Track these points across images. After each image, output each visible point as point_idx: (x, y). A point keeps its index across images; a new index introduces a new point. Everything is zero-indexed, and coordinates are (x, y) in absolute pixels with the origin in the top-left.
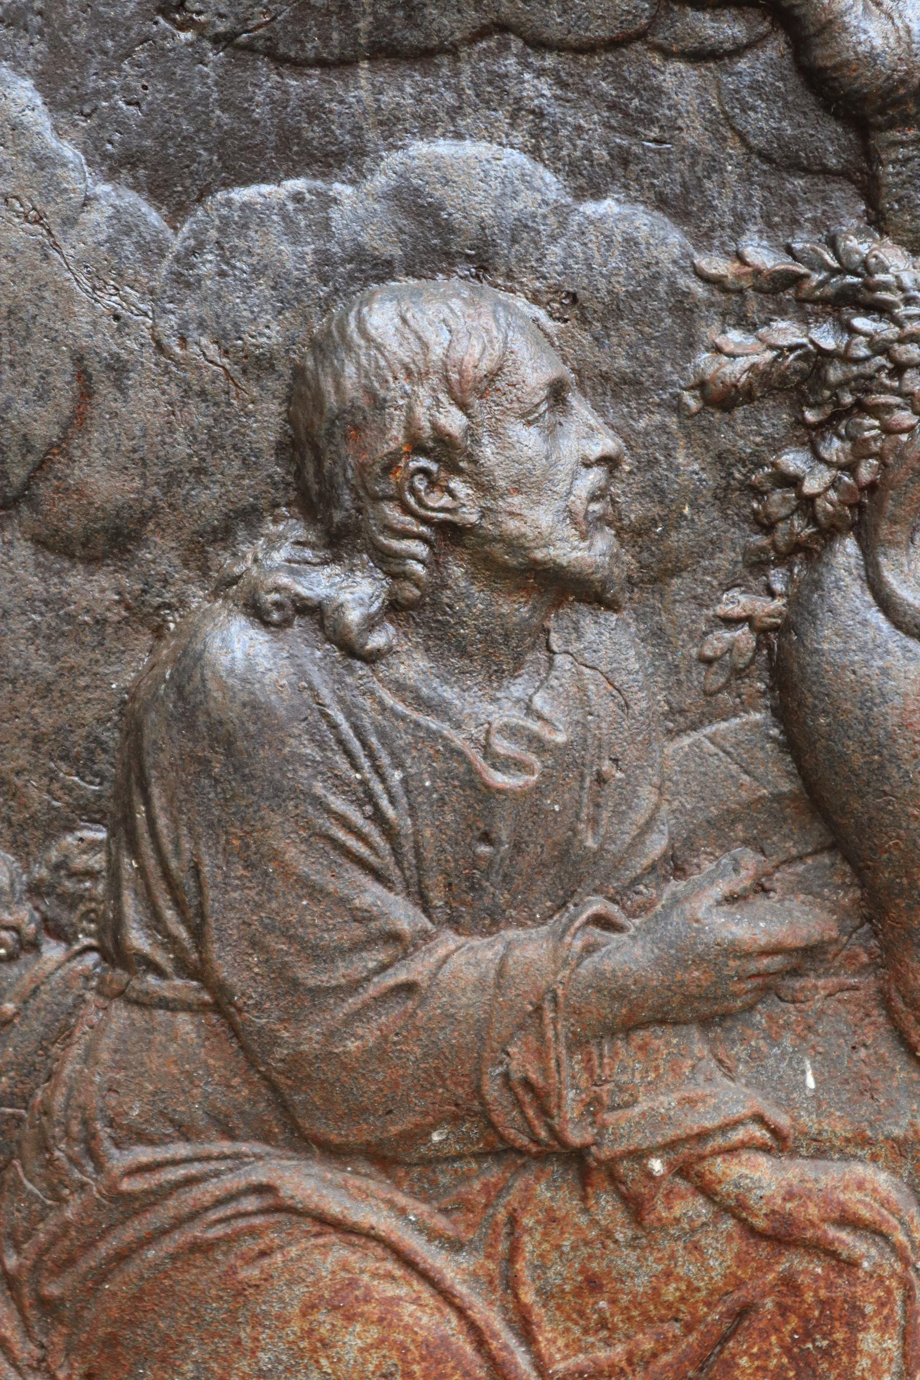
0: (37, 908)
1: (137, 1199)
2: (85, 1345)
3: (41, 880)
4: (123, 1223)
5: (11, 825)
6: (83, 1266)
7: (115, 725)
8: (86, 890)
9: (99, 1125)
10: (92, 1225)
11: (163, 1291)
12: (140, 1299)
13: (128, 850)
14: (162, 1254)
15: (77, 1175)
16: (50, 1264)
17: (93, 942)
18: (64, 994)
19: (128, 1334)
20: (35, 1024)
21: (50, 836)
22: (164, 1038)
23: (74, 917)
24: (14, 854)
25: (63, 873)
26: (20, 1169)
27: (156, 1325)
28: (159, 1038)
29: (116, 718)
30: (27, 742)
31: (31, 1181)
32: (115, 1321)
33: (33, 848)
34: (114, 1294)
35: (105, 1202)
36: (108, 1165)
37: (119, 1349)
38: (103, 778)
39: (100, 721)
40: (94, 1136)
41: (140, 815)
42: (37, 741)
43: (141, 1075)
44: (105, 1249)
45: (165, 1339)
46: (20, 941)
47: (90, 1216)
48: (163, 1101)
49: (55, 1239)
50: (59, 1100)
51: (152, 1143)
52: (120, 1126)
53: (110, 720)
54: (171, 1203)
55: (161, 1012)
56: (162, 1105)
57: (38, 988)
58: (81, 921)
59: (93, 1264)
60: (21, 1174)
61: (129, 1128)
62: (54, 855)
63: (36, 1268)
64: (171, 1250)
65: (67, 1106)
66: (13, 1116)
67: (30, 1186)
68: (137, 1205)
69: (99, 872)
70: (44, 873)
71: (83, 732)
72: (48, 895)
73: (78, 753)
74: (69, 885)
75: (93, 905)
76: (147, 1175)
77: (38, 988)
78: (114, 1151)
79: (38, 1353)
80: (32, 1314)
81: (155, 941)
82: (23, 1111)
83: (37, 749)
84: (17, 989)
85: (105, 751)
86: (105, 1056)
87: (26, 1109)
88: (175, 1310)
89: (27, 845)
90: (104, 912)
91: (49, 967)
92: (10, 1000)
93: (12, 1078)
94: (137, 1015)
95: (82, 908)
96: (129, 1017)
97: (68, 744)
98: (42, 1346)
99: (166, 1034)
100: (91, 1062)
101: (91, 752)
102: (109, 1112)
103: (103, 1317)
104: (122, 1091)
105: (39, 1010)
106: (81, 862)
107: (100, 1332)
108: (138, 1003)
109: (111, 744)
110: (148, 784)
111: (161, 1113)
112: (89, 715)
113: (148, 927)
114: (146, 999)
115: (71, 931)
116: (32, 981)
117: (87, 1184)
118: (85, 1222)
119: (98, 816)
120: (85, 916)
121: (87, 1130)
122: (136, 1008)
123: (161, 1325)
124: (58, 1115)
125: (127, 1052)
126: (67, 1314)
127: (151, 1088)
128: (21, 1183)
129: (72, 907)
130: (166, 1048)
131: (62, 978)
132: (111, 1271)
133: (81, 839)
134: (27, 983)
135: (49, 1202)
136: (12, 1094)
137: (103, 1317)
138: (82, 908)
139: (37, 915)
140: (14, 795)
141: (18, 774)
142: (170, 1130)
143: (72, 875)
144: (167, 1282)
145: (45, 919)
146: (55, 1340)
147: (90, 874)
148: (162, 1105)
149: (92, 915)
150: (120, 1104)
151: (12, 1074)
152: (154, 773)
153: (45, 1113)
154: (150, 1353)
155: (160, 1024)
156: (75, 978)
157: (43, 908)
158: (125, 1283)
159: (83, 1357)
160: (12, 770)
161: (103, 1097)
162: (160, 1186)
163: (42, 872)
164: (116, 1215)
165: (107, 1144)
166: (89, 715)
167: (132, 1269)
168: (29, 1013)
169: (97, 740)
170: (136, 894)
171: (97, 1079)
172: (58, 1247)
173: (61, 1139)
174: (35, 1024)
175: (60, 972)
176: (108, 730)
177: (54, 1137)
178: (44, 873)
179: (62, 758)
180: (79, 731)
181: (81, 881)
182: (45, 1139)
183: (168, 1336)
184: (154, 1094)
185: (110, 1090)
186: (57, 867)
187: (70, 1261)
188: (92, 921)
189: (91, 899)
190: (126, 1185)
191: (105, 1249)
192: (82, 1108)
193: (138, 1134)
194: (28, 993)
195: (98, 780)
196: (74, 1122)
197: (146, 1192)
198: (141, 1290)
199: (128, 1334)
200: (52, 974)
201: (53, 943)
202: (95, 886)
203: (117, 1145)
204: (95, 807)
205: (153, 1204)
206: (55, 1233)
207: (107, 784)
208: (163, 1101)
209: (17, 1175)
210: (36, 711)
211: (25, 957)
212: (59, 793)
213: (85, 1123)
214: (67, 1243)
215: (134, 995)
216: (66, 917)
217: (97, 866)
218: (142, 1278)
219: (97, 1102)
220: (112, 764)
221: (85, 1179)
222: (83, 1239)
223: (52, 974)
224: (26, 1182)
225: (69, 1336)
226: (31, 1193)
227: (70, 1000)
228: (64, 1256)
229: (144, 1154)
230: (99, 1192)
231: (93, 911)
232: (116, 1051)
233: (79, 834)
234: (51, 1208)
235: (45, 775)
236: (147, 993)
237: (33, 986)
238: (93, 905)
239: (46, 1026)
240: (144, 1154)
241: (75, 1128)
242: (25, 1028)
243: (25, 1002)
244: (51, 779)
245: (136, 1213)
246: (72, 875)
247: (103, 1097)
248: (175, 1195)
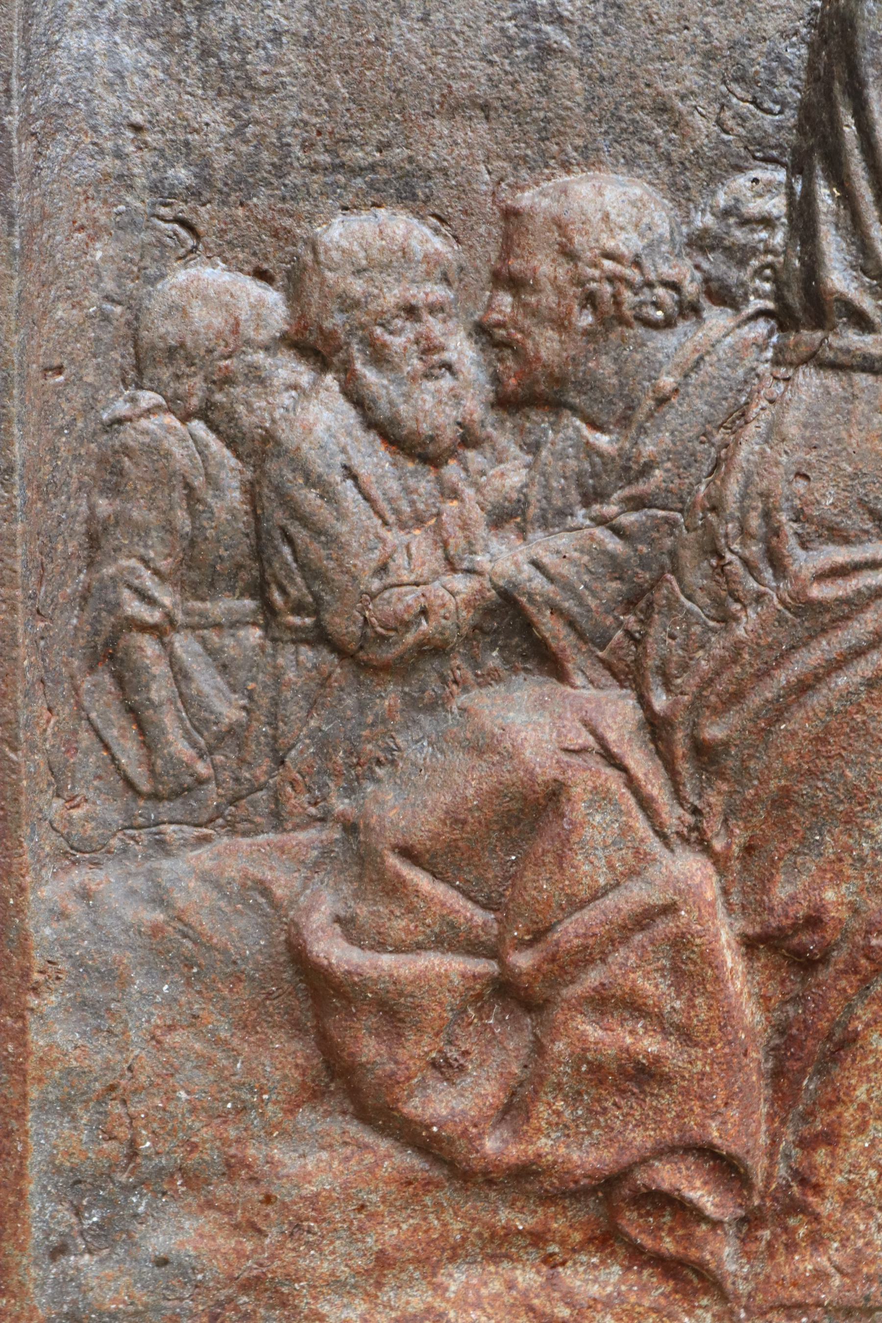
0: (697, 267)
1: (828, 610)
2: (751, 804)
3: (706, 230)
4: (806, 645)
5: (670, 163)
6: (754, 701)
7: (803, 40)
8: (761, 241)
9: (784, 517)
10: (770, 647)
11: (853, 730)
12: (824, 741)
13: (827, 178)
14: (857, 679)
15: (753, 584)
16: (713, 698)
17: (770, 305)
18: (733, 367)
19: (805, 789)
20: (699, 404)
21: (715, 179)
22: (867, 409)
23: (745, 275)
24: (672, 200)
25: (732, 221)
26: (675, 583)
27: (842, 775)
28: (861, 407)
29: (804, 31)
30: (697, 58)
31: (689, 598)
32: (791, 772)
33: (694, 193)
34: (794, 734)
35: (789, 615)
36: (794, 568)
37: (791, 811)
38: (784, 105)
39: (784, 34)
40: (776, 532)
41: (850, 130)
42: (710, 55)
43: (837, 454)
44: (783, 677)
45: (852, 793)
46: (680, 303)
47: (768, 634)
48: (864, 485)
49: (723, 665)
50: (733, 488)
51: (846, 541)
52: (809, 520)
53: (796, 34)
54: (869, 616)
55: (864, 375)
56: (862, 491)
57: (702, 358)
58: (752, 279)
59: (769, 695)
60: (677, 589)
61: (821, 523)
62: (722, 200)
63: (697, 706)
64: (869, 674)
65: (745, 496)
66: (666, 520)
67: (688, 604)
68: (827, 618)
69: (778, 218)
70: (709, 220)
71: (764, 47)
72: (712, 249)
73: (757, 72)
74: (740, 235)
75: (770, 258)
76: (840, 581)
77: (702, 358)
78: (799, 552)
79: (689, 819)
80: (685, 767)
81: (863, 285)
82: (678, 515)
83: (706, 67)
84: (677, 360)
85: (789, 72)
86: (793, 431)
87: (681, 511)
88: (867, 754)
89: (687, 188)
90: (787, 263)
91: (714, 334)
92: (668, 373)
93: (667, 471)
94: (833, 382)
95: (755, 263)
96: (822, 384)
97: (744, 61)
98: (695, 811)
99: (869, 403)
100: (774, 440)
101: (771, 71)
102: (797, 502)
103: (777, 765)
104: (812, 475)
105: (703, 385)
106: (755, 207)
107: (773, 785)
108: (835, 366)
109: (797, 62)
110: (863, 84)
111: (861, 502)
112: (770, 27)
113: (853, 267)
114: (843, 359)
115: (741, 292)
116: (696, 350)
117: (764, 594)
118: (762, 642)
119: (775, 153)
120: (758, 273)
121: (767, 524)
122: (830, 373)
123: (847, 772)
124: (732, 505)
125: (819, 426)
126: (730, 763)
127: (850, 469)
128: (677, 600)
129: (742, 263)
130: (869, 420)
131: (731, 347)
132: (787, 707)
133: (756, 181)
134: (688, 354)
135: (712, 624)
136: (668, 490)
137: (777, 765)
138: (755, 263)
139: (698, 275)
140: (676, 125)
141: (683, 98)
142: (869, 526)
143: (745, 222)
144: (859, 718)
145: (707, 280)
146: (712, 800)
147: (767, 222)
148: (862, 491)
149: (768, 272)
150: (811, 491)
151: (669, 465)
152: (871, 71)
153: (714, 509)
154: (832, 812)
155: (862, 391)
156: (746, 347)
157: (705, 266)
158: (808, 719)
159: (746, 820)
160: (677, 93)
161: (790, 483)
162: (859, 592)
163: (704, 220)
164: (801, 633)
165: (793, 541)
166: (770, 27)
167: (817, 701)
168: (691, 389)
169: (779, 58)
170: (837, 228)
171: (784, 459)
172: (725, 677)
173: (735, 538)
174: (699, 404)
175: (729, 339)
176: (793, 45)
177: (726, 536)
178: (709, 220)
179: (736, 80)
180: (759, 46)
181: (753, 231)
182: (714, 539)
183: (857, 787)
184: (854, 477)
185: (798, 474)
186: (727, 213)
187: (737, 697)
188: (767, 279)
189: (767, 251)
190: (816, 592)
191: (783, 677)
192: (765, 496)
193: (830, 529)
194: (690, 364)
195: (777, 108)
196: (754, 514)
197: (842, 601)
198: (827, 729)
199: (805, 789)
200: (719, 341)
201: (716, 309)
202: (772, 235)
203: (804, 546)
204: (773, 141)
205: (847, 618)
206: (723, 658)
207: (788, 113)
208: (864, 485)
209: (672, 592)
210: (709, 19)
211: (683, 326)
212: (730, 123)
213: (767, 515)
214: (739, 669)
215: (830, 355)
216: (733, 275)
217: (775, 212)
218: (830, 711)
219: (782, 488)
220: (796, 87)
221: (762, 588)
222: (758, 664)
223: (719, 341)
224: (683, 598)
225: (730, 794)
226: (689, 612)
227: (741, 372)
228: (732, 688)
229: (841, 555)
230: (782, 601)
231: (770, 266)
232: (805, 426)
233: (753, 174)
234: (714, 630)
235: (716, 100)
236: (848, 351)
237: (696, 356)
238: (770, 258)
239: (712, 406)
240: (841, 555)
241: (755, 522)
242: (685, 408)
243: (686, 376)
244: (722, 107)
245: (824, 631)
246: (745, 222)
247: (790, 483)
248: (873, 606)
